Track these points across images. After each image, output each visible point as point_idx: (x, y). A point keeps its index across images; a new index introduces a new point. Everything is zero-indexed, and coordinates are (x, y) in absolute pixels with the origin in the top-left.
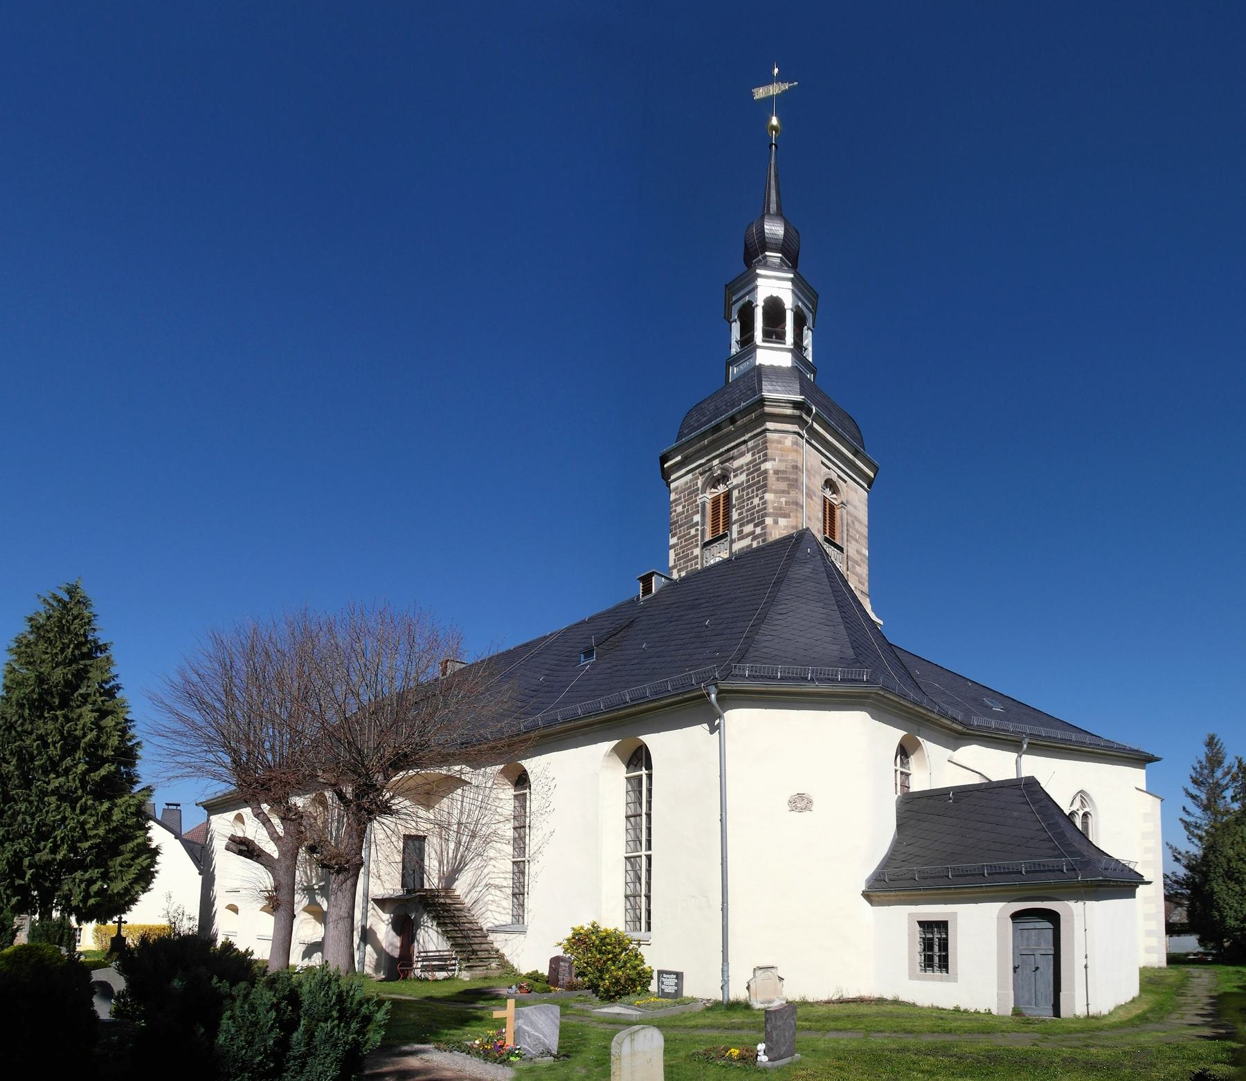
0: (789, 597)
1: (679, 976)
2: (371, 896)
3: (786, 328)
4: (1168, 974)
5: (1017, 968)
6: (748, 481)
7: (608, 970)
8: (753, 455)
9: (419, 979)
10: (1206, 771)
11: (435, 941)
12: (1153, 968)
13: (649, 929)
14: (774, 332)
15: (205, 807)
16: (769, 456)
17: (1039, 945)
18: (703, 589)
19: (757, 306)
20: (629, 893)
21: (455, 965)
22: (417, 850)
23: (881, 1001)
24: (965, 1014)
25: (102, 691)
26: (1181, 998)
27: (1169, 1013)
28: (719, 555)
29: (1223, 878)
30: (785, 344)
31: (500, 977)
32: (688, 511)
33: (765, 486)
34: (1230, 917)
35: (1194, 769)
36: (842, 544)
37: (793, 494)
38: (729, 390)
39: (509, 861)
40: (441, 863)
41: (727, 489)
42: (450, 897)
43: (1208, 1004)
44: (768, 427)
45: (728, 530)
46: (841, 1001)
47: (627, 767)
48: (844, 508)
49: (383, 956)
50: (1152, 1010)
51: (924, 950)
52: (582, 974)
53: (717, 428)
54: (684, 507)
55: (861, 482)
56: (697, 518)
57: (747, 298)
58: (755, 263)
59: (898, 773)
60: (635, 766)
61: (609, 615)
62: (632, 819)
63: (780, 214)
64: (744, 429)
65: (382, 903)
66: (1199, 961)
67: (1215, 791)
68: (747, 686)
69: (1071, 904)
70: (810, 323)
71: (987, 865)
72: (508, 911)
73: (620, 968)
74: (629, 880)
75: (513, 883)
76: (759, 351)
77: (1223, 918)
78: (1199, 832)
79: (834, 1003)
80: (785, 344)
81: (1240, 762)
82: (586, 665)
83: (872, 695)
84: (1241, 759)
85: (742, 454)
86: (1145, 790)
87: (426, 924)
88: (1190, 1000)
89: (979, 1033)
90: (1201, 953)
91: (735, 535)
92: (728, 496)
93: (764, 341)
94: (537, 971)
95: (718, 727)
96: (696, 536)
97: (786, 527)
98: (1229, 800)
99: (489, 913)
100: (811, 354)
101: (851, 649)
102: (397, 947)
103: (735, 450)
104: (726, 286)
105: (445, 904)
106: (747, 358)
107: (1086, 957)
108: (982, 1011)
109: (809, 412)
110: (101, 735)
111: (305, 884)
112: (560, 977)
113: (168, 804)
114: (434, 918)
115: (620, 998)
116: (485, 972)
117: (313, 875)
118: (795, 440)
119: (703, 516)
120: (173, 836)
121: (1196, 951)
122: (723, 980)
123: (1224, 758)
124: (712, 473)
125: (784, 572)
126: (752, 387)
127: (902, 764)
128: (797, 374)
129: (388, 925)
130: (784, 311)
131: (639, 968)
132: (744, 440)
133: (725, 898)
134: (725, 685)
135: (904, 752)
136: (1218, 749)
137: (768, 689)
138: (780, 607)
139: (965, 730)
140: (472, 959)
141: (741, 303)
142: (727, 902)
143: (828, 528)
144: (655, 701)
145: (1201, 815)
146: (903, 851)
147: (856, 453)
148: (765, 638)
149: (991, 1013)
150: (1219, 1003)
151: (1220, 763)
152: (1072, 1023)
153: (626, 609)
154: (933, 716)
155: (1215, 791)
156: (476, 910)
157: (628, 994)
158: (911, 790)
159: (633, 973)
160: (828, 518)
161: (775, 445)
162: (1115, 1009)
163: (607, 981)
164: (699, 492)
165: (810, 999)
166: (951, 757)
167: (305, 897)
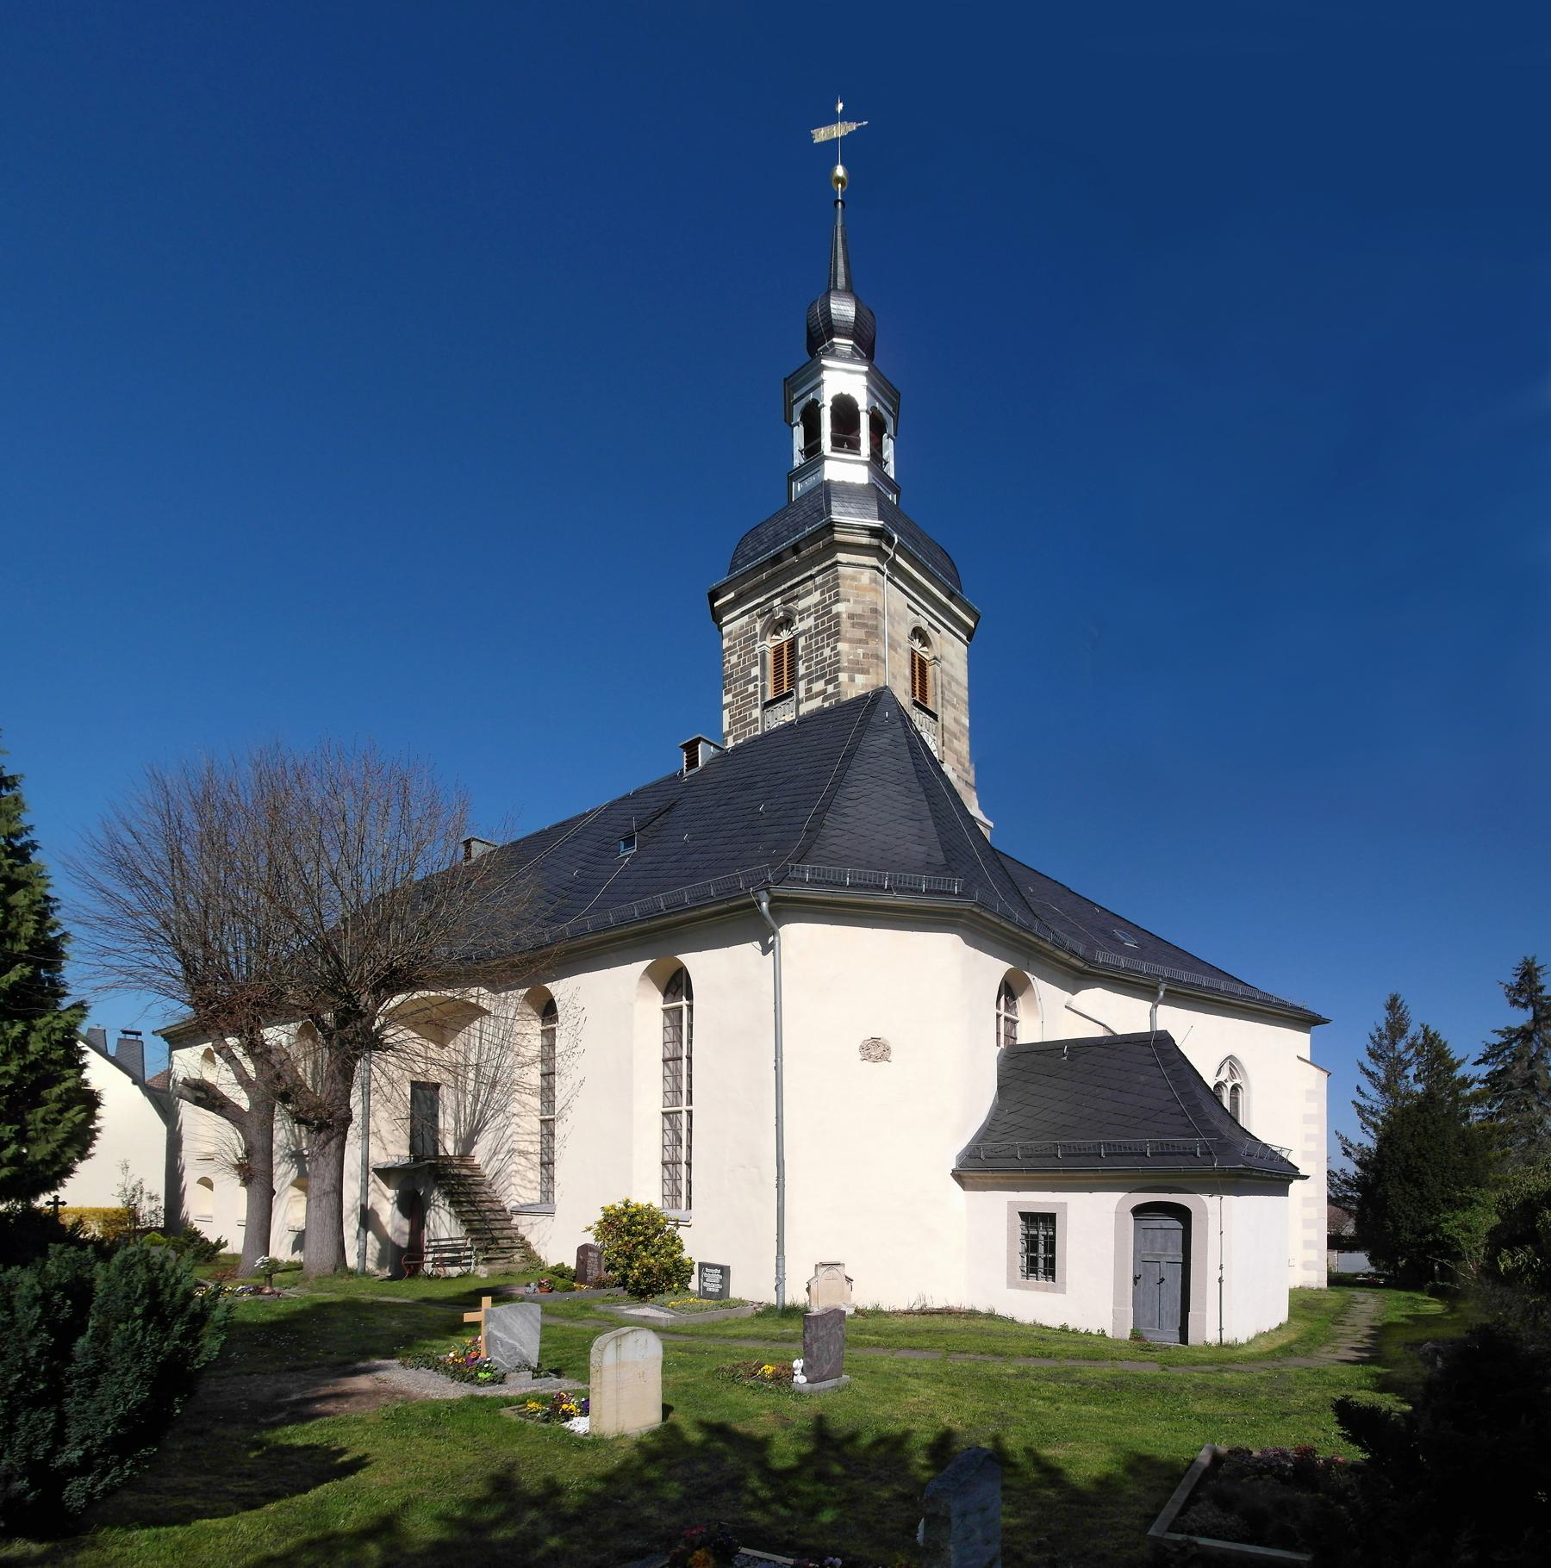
0: (862, 777)
1: (724, 1271)
2: (372, 1165)
3: (861, 435)
4: (1328, 1297)
5: (1139, 1278)
6: (816, 626)
7: (638, 1256)
8: (822, 593)
9: (429, 1277)
10: (1386, 1042)
11: (448, 1225)
12: (1312, 1289)
13: (689, 1206)
14: (846, 438)
15: (166, 1037)
16: (842, 596)
17: (1165, 1250)
18: (759, 762)
19: (823, 406)
20: (667, 1158)
21: (470, 1257)
22: (429, 1102)
23: (972, 1314)
24: (1073, 1335)
25: (9, 849)
26: (1337, 1327)
27: (1320, 1346)
28: (783, 718)
29: (1400, 1179)
30: (859, 455)
31: (524, 1273)
32: (744, 663)
33: (837, 633)
34: (1406, 1229)
35: (1372, 1038)
36: (936, 711)
37: (872, 644)
38: (791, 511)
39: (535, 1119)
40: (457, 1121)
41: (792, 636)
42: (467, 1167)
43: (1367, 1337)
44: (839, 560)
45: (793, 687)
46: (924, 1312)
47: (665, 995)
48: (938, 665)
49: (389, 1247)
50: (1300, 1341)
51: (1027, 1251)
52: (611, 1267)
53: (777, 559)
54: (739, 657)
55: (958, 632)
56: (756, 671)
57: (811, 396)
58: (821, 351)
59: (1002, 1018)
60: (675, 994)
61: (657, 789)
62: (670, 1063)
63: (850, 290)
64: (810, 561)
65: (385, 1174)
66: (1368, 1283)
67: (1396, 1067)
68: (809, 894)
69: (1205, 1198)
70: (890, 429)
71: (1104, 1143)
72: (535, 1185)
73: (653, 1255)
74: (667, 1142)
75: (541, 1149)
76: (827, 463)
77: (1397, 1229)
78: (1374, 1119)
79: (915, 1314)
80: (859, 455)
81: (1426, 1031)
82: (625, 857)
83: (965, 913)
84: (1427, 1026)
85: (809, 593)
86: (1309, 1060)
87: (436, 1203)
88: (1348, 1330)
89: (1084, 1359)
90: (1372, 1274)
91: (802, 694)
92: (793, 644)
93: (833, 450)
94: (563, 1264)
95: (772, 946)
96: (755, 693)
97: (864, 686)
98: (1411, 1079)
99: (513, 1187)
100: (892, 469)
101: (942, 853)
102: (404, 1233)
103: (801, 587)
104: (785, 379)
105: (458, 1176)
106: (812, 472)
107: (1221, 1268)
108: (1095, 1332)
109: (890, 542)
110: (10, 919)
111: (294, 1149)
112: (589, 1271)
113: (125, 1032)
114: (446, 1195)
115: (653, 1296)
116: (506, 1266)
117: (303, 1135)
118: (874, 577)
119: (763, 669)
120: (130, 1080)
121: (1366, 1272)
122: (777, 1278)
123: (1408, 1025)
124: (773, 616)
125: (855, 743)
126: (818, 508)
127: (1007, 1008)
128: (874, 492)
129: (393, 1204)
130: (857, 414)
131: (676, 1256)
132: (811, 575)
133: (781, 1170)
134: (780, 891)
135: (1010, 990)
136: (1402, 1014)
137: (877, 901)
138: (850, 790)
139: (1086, 967)
140: (491, 1249)
141: (803, 402)
142: (783, 1177)
143: (917, 689)
144: (694, 909)
145: (1378, 1098)
146: (1004, 1120)
147: (951, 596)
148: (833, 833)
149: (1105, 1335)
150: (1381, 1332)
151: (1403, 1032)
152: (1201, 1352)
153: (666, 788)
154: (1046, 946)
155: (1396, 1067)
156: (497, 1184)
157: (663, 1292)
158: (1018, 1042)
159: (667, 1261)
160: (917, 677)
161: (848, 582)
162: (1256, 1337)
163: (636, 1271)
164: (758, 639)
165: (885, 1308)
166: (1069, 1002)
167: (293, 1166)
